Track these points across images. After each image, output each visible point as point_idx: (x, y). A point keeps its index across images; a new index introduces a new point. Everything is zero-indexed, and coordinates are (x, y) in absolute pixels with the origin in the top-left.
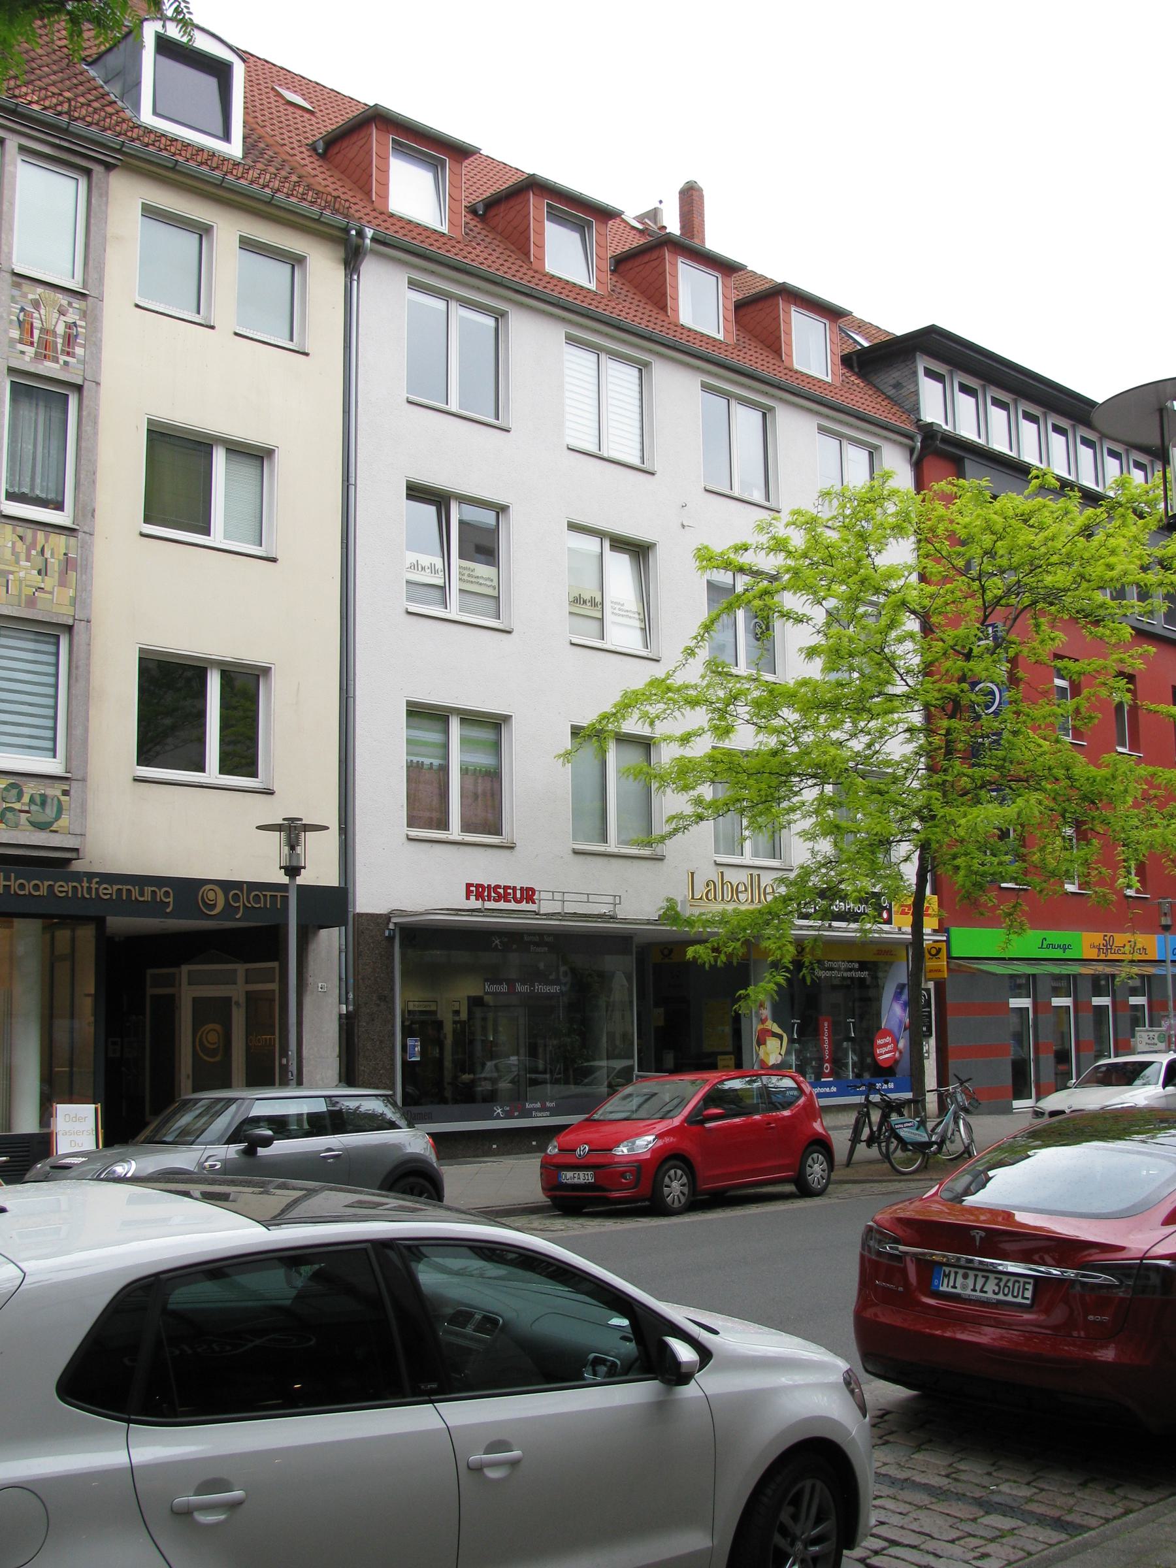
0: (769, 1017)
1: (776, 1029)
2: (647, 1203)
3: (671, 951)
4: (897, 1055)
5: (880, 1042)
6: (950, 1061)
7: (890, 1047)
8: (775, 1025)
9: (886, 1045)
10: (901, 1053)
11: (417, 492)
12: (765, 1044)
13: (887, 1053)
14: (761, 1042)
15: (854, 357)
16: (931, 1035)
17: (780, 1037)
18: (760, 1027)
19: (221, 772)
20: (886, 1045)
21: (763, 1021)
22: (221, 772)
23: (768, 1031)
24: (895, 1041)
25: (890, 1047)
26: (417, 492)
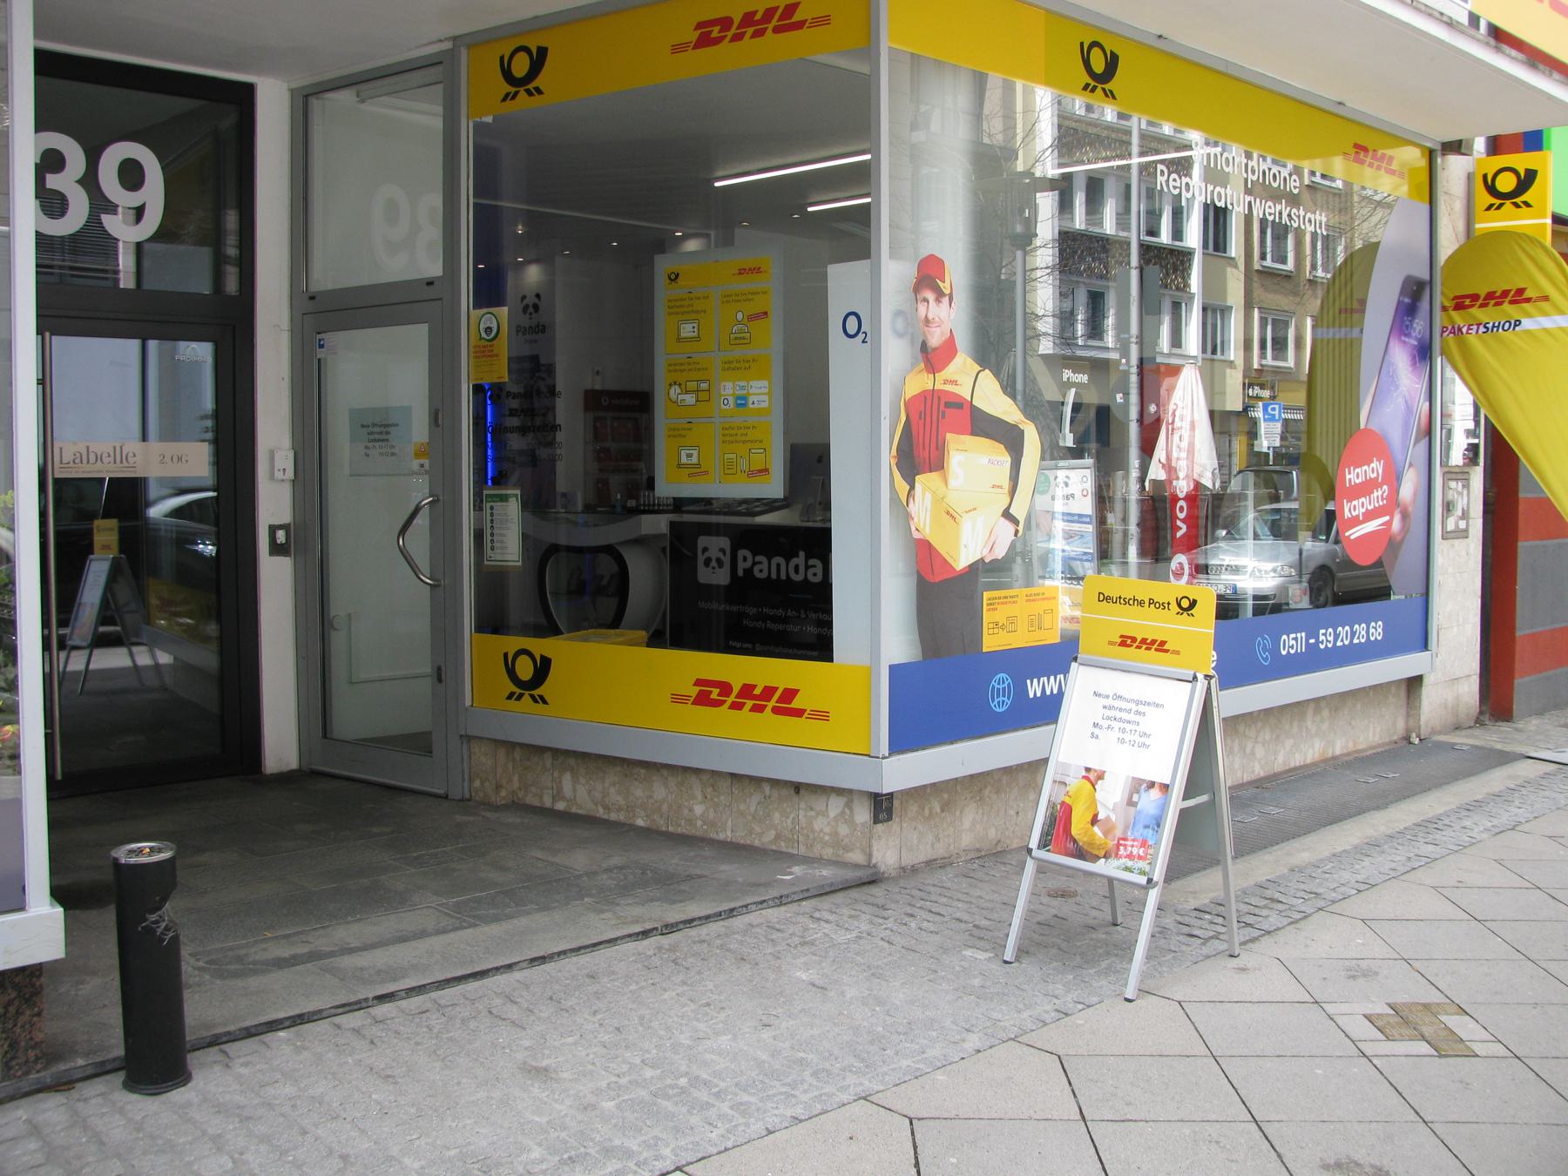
0: (963, 341)
1: (992, 399)
2: (468, 703)
3: (539, 60)
4: (1396, 525)
5: (1354, 476)
6: (1524, 546)
7: (1378, 496)
8: (988, 382)
9: (1366, 488)
10: (1405, 516)
11: (504, 100)
12: (937, 463)
13: (1369, 516)
14: (919, 455)
15: (864, 69)
16: (1477, 464)
17: (1011, 439)
18: (920, 382)
19: (891, 667)
20: (1366, 488)
21: (933, 358)
22: (891, 667)
23: (957, 403)
24: (1393, 478)
25: (1378, 496)
26: (504, 100)
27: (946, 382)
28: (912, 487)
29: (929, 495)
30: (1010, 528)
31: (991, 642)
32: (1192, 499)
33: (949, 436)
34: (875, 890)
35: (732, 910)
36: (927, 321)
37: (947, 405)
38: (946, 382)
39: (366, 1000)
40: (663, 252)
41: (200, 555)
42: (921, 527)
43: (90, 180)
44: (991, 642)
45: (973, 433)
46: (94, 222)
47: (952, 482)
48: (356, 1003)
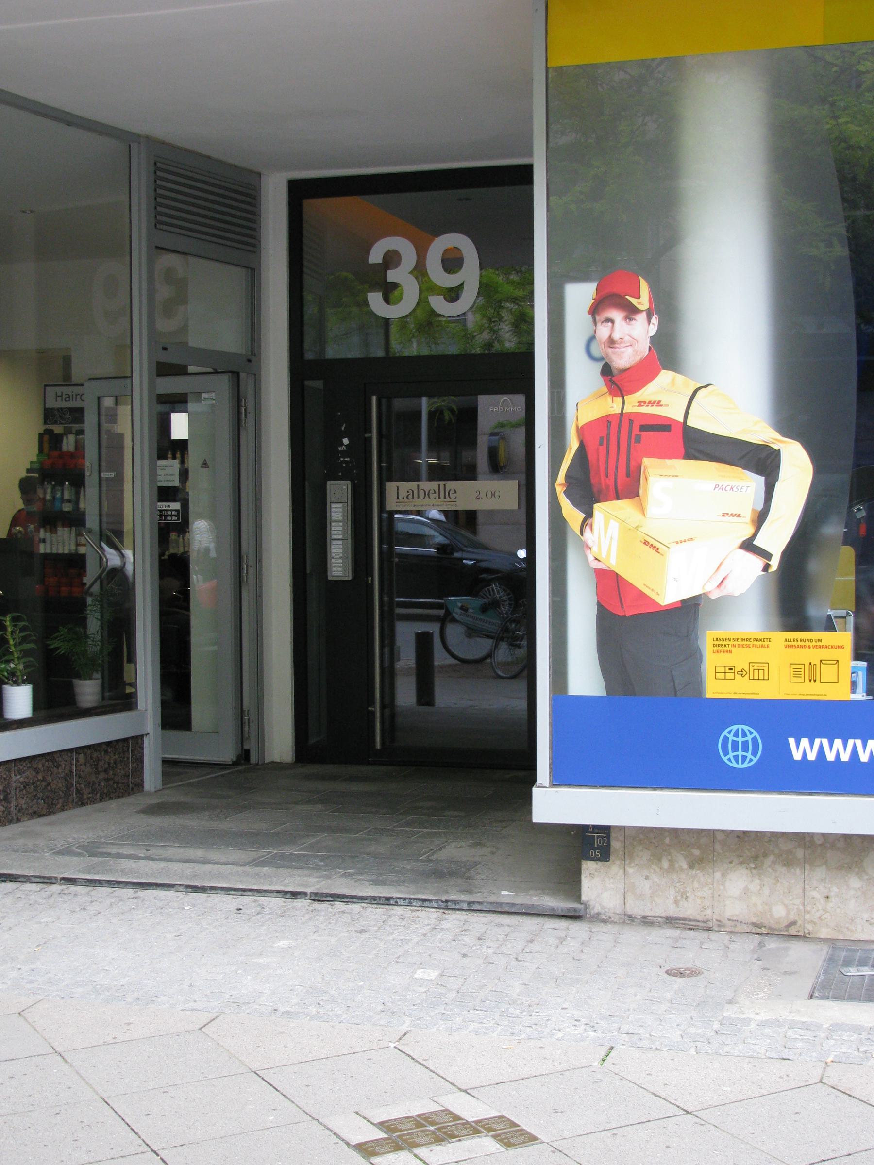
12: (629, 488)
27: (641, 404)
28: (589, 515)
29: (614, 526)
30: (758, 563)
31: (716, 687)
32: (198, 551)
33: (646, 461)
34: (575, 927)
35: (388, 899)
36: (611, 342)
37: (644, 428)
38: (641, 404)
39: (56, 878)
40: (187, 343)
41: (467, 565)
42: (603, 556)
43: (420, 271)
44: (716, 687)
45: (688, 456)
46: (422, 302)
47: (652, 509)
48: (49, 878)
